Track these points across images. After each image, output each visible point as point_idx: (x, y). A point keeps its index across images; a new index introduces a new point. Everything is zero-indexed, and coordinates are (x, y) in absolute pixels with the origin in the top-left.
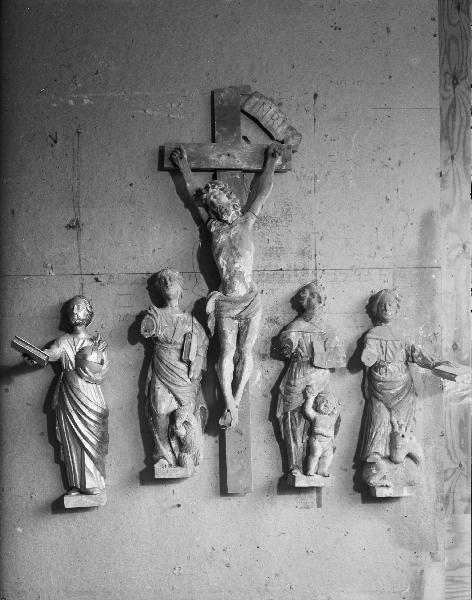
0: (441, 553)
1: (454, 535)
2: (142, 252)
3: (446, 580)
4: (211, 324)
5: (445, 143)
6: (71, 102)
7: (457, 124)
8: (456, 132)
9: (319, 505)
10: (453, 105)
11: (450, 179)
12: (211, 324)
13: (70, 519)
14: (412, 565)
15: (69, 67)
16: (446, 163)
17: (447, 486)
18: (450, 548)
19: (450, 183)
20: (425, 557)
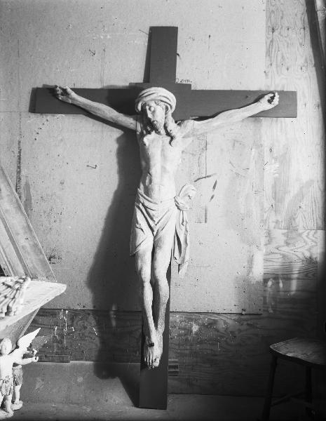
0: (262, 246)
1: (268, 238)
2: (85, 397)
3: (273, 298)
4: (155, 233)
5: (268, 58)
6: (102, 37)
7: (273, 50)
8: (273, 53)
9: (206, 222)
10: (272, 41)
11: (270, 74)
12: (155, 233)
13: (100, 129)
14: (248, 251)
15: (101, 22)
16: (268, 67)
17: (265, 215)
18: (266, 245)
19: (270, 76)
20: (254, 248)
